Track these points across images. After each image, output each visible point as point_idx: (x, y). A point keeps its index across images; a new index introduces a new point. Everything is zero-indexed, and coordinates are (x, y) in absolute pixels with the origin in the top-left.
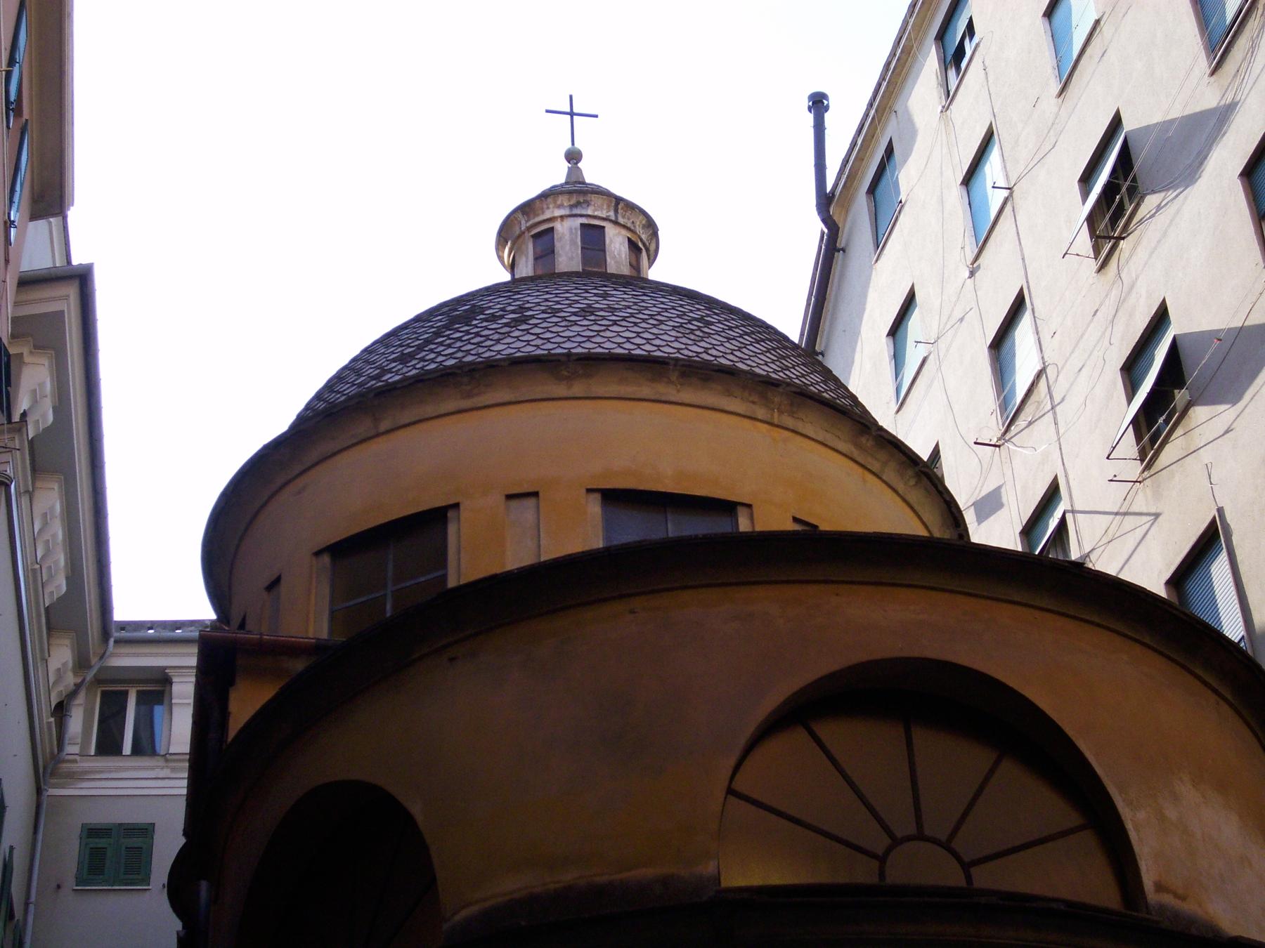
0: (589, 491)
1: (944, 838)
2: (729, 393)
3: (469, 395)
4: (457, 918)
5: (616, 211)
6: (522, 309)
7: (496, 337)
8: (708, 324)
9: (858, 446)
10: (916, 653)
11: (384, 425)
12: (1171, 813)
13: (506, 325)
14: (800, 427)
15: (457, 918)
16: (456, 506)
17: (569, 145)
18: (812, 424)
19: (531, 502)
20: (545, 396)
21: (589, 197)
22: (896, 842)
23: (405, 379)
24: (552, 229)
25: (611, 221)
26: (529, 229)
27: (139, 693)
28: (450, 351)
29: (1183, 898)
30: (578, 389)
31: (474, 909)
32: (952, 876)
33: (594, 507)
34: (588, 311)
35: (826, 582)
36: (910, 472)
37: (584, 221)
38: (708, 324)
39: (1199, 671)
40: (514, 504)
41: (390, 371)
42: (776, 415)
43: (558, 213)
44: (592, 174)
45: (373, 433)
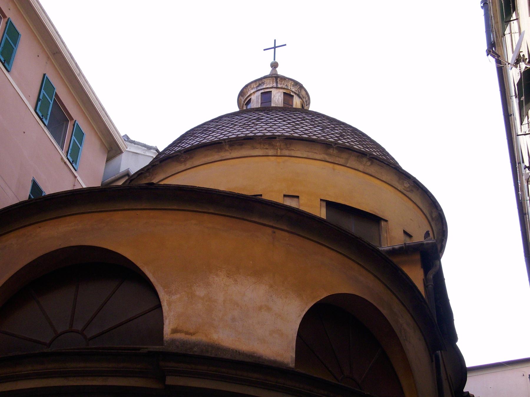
2: (254, 148)
5: (277, 83)
9: (327, 154)
14: (293, 153)
17: (273, 60)
18: (299, 151)
20: (177, 172)
21: (263, 81)
25: (275, 88)
36: (365, 160)
37: (263, 91)
42: (279, 151)
43: (252, 91)
44: (280, 71)
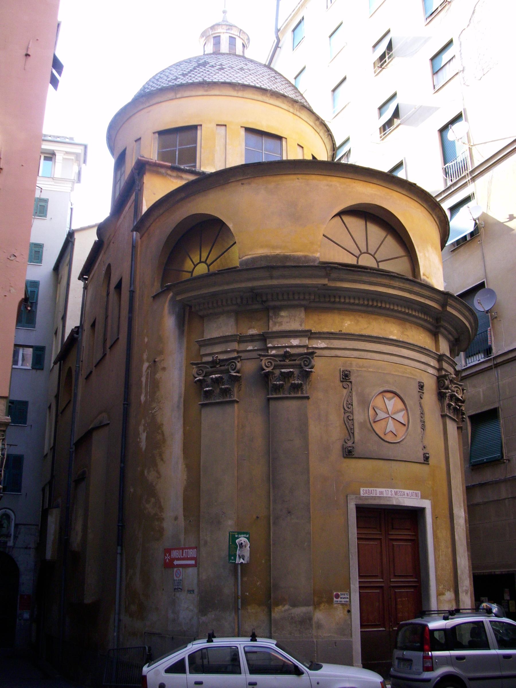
0: (242, 127)
1: (373, 254)
3: (206, 91)
4: (244, 258)
6: (221, 65)
7: (214, 73)
8: (276, 79)
9: (315, 124)
10: (373, 203)
11: (178, 96)
12: (427, 255)
13: (217, 69)
15: (244, 258)
16: (201, 125)
19: (224, 128)
21: (232, 27)
22: (362, 253)
23: (187, 83)
24: (219, 36)
26: (212, 34)
27: (45, 157)
28: (199, 75)
29: (428, 278)
30: (240, 94)
31: (249, 257)
32: (374, 265)
33: (243, 132)
34: (242, 69)
35: (352, 179)
36: (326, 134)
38: (276, 79)
39: (434, 216)
40: (219, 127)
41: (179, 78)
45: (174, 97)
